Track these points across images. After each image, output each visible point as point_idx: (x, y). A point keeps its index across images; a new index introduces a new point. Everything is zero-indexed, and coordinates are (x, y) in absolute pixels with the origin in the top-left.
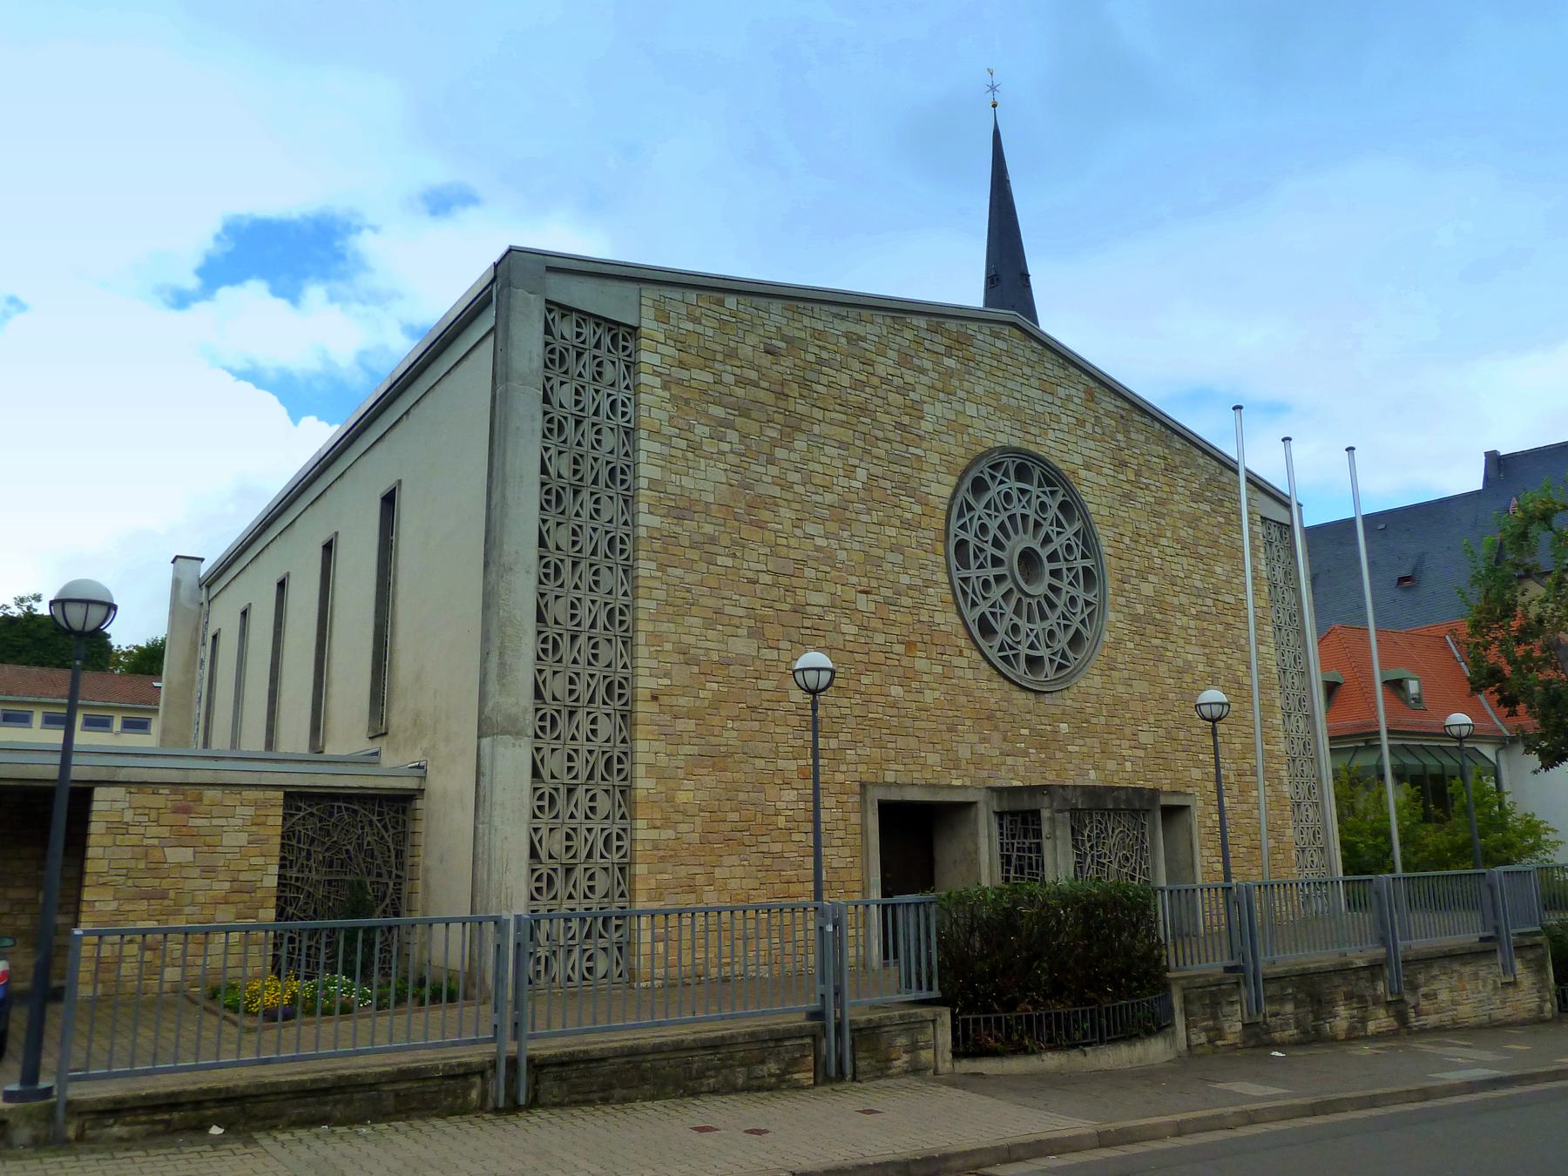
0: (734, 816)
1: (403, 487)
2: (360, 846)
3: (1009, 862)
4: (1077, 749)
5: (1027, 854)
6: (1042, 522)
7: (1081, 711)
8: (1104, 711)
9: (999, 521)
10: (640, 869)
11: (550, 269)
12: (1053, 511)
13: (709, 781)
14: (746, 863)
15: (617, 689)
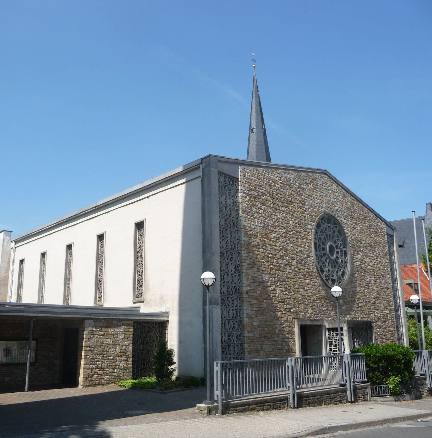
0: (266, 329)
3: (332, 344)
4: (344, 308)
5: (338, 341)
6: (334, 236)
8: (350, 296)
11: (219, 161)
12: (337, 233)
13: (260, 318)
14: (269, 343)
15: (238, 290)
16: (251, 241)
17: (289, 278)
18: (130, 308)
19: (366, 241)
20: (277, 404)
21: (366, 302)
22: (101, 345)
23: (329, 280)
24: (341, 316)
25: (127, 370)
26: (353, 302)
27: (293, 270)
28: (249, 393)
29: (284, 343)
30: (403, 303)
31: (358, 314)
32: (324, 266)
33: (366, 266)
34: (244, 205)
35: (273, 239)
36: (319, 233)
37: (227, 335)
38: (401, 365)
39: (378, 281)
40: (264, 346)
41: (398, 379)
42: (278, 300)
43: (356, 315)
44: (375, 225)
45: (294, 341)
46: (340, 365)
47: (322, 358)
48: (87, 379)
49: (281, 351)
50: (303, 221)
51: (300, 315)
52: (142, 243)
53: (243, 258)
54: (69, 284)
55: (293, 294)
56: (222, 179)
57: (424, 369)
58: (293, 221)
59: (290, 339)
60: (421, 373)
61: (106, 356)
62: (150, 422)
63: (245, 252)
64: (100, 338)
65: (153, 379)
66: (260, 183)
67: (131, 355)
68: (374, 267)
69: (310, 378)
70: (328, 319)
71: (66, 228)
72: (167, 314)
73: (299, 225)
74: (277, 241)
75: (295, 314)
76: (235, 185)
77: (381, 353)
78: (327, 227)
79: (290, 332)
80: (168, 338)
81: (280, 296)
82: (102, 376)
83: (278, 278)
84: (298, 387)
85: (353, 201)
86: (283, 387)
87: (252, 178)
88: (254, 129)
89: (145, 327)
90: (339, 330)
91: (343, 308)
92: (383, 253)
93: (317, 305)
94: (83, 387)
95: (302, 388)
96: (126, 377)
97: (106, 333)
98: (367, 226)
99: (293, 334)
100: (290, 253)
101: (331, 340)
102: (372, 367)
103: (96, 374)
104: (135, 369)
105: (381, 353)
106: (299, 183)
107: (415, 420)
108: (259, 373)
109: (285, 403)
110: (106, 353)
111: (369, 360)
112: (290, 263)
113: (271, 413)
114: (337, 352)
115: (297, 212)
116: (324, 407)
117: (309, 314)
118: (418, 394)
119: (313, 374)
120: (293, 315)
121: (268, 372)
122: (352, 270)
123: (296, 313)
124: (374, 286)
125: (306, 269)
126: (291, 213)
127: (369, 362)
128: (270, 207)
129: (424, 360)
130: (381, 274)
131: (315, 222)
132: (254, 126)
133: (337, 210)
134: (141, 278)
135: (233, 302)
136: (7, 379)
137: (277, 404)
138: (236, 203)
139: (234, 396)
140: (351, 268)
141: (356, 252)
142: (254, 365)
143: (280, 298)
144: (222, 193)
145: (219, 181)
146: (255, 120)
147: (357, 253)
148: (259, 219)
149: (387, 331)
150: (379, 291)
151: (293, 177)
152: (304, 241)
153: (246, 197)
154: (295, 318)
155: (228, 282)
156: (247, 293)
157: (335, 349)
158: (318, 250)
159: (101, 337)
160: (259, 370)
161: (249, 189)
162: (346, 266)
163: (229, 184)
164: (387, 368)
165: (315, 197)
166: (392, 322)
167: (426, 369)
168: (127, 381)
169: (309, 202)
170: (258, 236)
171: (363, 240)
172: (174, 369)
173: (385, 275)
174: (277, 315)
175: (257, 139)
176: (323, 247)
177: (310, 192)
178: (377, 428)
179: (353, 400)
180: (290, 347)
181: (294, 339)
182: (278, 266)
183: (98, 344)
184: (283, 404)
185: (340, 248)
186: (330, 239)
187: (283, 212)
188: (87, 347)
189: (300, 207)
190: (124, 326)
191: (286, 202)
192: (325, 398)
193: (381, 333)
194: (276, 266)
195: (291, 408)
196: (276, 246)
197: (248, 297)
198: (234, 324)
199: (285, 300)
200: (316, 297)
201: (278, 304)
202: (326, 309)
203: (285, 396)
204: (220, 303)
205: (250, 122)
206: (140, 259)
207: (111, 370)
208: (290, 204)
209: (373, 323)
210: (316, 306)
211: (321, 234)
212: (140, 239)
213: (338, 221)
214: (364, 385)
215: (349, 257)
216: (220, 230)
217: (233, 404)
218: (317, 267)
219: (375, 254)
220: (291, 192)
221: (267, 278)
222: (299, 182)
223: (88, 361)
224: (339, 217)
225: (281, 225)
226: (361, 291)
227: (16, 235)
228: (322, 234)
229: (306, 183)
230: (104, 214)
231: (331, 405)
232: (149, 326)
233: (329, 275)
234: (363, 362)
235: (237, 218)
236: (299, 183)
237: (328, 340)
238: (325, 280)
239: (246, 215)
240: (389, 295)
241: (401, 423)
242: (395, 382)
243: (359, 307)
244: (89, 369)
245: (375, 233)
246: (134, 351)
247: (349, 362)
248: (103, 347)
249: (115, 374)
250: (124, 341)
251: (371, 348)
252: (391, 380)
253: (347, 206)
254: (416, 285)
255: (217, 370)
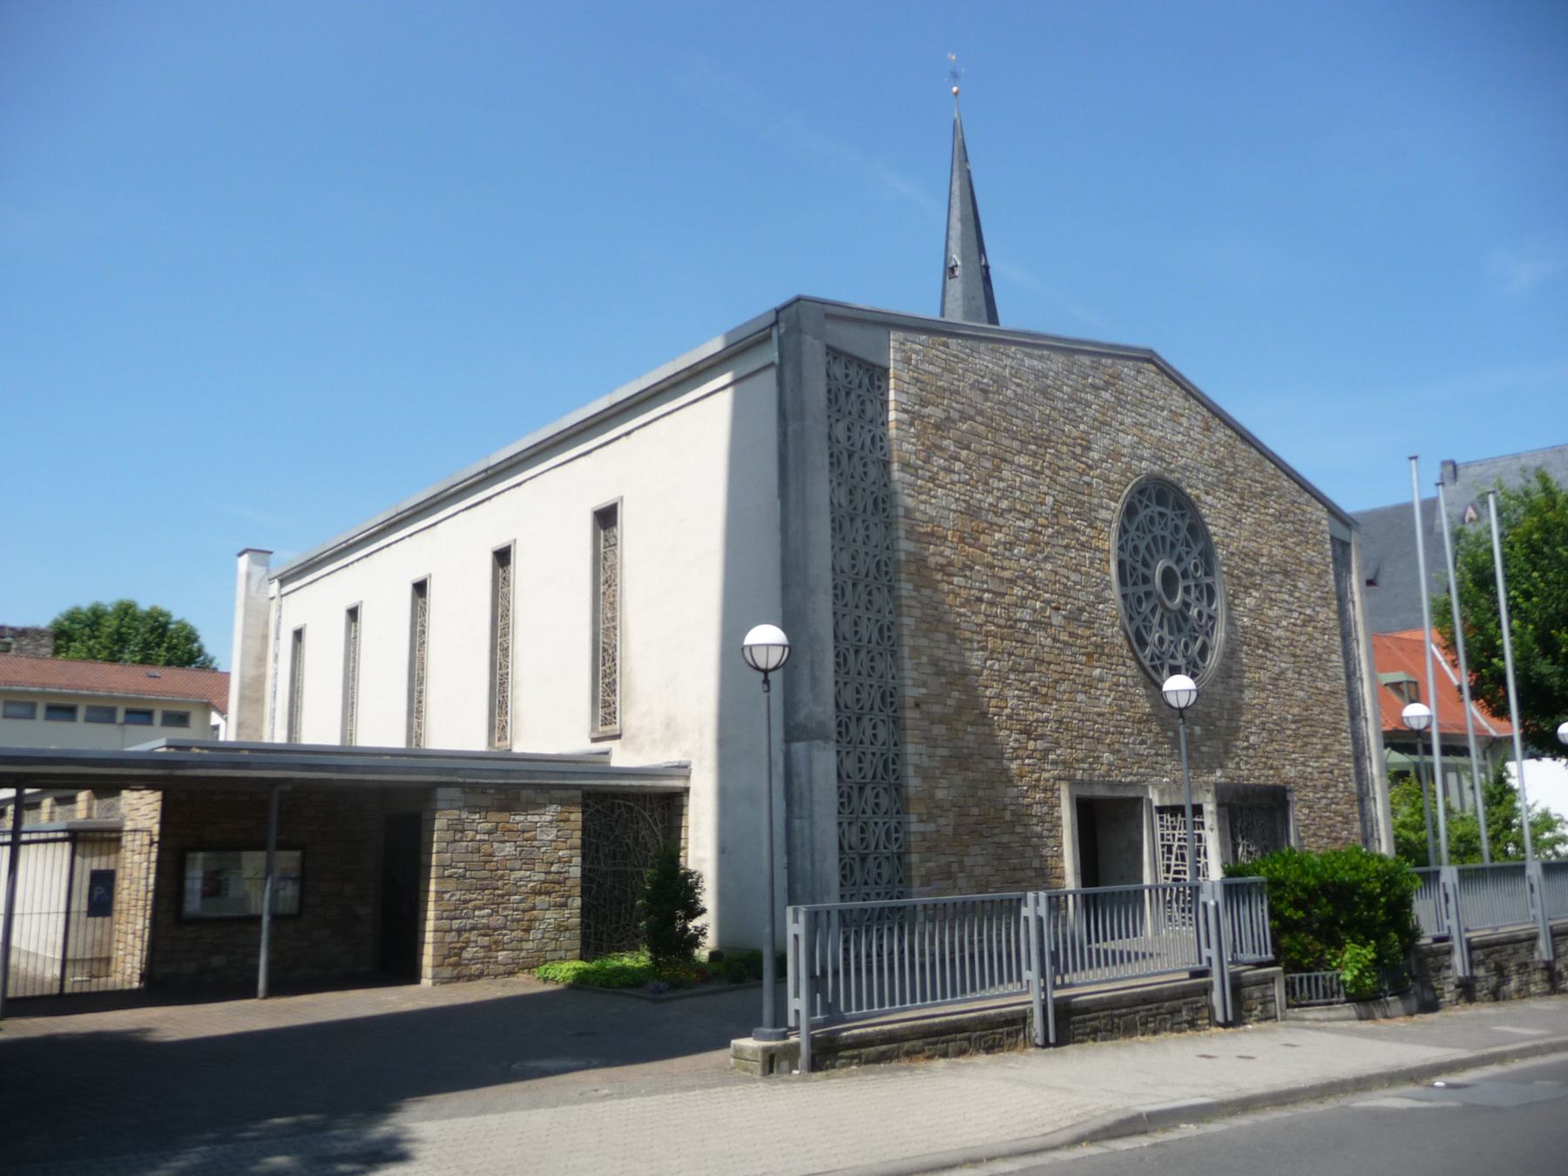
0: (975, 811)
1: (625, 502)
2: (636, 839)
3: (1170, 850)
7: (1208, 714)
9: (1146, 541)
10: (914, 858)
11: (829, 316)
12: (1184, 532)
13: (958, 779)
15: (890, 698)
16: (927, 554)
17: (1043, 661)
18: (582, 756)
19: (1270, 556)
20: (992, 1034)
21: (1270, 731)
22: (486, 862)
23: (1163, 669)
24: (1198, 772)
25: (567, 934)
26: (1233, 731)
27: (1055, 640)
28: (903, 1001)
29: (1029, 852)
30: (1377, 734)
31: (1248, 766)
32: (1149, 629)
33: (1270, 628)
34: (906, 446)
35: (996, 547)
36: (1132, 533)
37: (855, 829)
38: (1376, 912)
39: (1305, 671)
40: (968, 861)
41: (1369, 953)
42: (1012, 725)
43: (1240, 769)
44: (1298, 511)
45: (1060, 845)
46: (1190, 912)
47: (1143, 892)
48: (447, 961)
49: (1019, 875)
50: (1086, 498)
51: (1076, 769)
52: (613, 567)
53: (904, 602)
54: (421, 692)
55: (1056, 710)
56: (838, 370)
57: (1447, 923)
58: (1054, 496)
59: (1048, 837)
60: (1436, 933)
61: (500, 892)
62: (567, 1101)
63: (910, 586)
64: (484, 841)
65: (637, 960)
66: (955, 382)
67: (579, 889)
68: (1293, 632)
69: (1106, 952)
70: (1161, 782)
71: (410, 535)
72: (683, 769)
73: (1072, 510)
74: (1007, 553)
75: (1061, 767)
76: (879, 387)
77: (1316, 876)
78: (1156, 517)
79: (1048, 818)
80: (687, 838)
81: (1017, 714)
82: (490, 950)
83: (1010, 663)
84: (1059, 981)
85: (1231, 441)
86: (1010, 980)
87: (931, 368)
88: (956, 266)
89: (620, 808)
90: (1188, 812)
91: (1204, 749)
92: (1318, 593)
93: (1126, 741)
94: (434, 984)
95: (1071, 985)
96: (562, 953)
97: (500, 825)
98: (1272, 515)
99: (1056, 825)
100: (1046, 588)
101: (1169, 840)
102: (1290, 918)
103: (472, 945)
104: (592, 931)
105: (1316, 876)
106: (1071, 387)
107: (1425, 1082)
108: (954, 936)
109: (1017, 1032)
110: (500, 883)
111: (1281, 899)
112: (1046, 620)
113: (972, 1064)
114: (1185, 874)
115: (1068, 469)
116: (1143, 1042)
117: (1105, 768)
118: (1428, 996)
119: (1113, 938)
120: (1055, 767)
121: (980, 934)
122: (1228, 640)
123: (1064, 762)
124: (1294, 685)
125: (1094, 635)
126: (1047, 472)
127: (1281, 902)
128: (986, 453)
129: (1446, 896)
130: (1315, 652)
131: (1121, 500)
132: (956, 259)
133: (1185, 468)
134: (613, 669)
135: (874, 732)
136: (217, 961)
137: (992, 1034)
138: (881, 440)
139: (854, 1012)
140: (1228, 635)
141: (1242, 589)
142: (936, 913)
143: (1017, 720)
144: (839, 411)
145: (828, 375)
146: (959, 243)
147: (1245, 592)
148: (951, 490)
149: (1332, 815)
150: (1310, 701)
151: (1055, 368)
152: (1087, 555)
153: (912, 424)
154: (1059, 779)
155: (859, 674)
156: (917, 705)
157: (1181, 868)
158: (1130, 582)
159: (486, 837)
160: (952, 929)
161: (921, 400)
162: (1212, 628)
163: (860, 386)
164: (1333, 921)
165: (1121, 428)
166: (1346, 788)
167: (1452, 922)
168: (562, 966)
169: (1101, 442)
170: (950, 538)
171: (1262, 555)
172: (703, 929)
173: (1325, 656)
174: (1008, 769)
175: (965, 296)
176: (1143, 574)
177: (1103, 414)
178: (1305, 1111)
179: (1230, 1018)
180: (1046, 861)
181: (1058, 839)
182: (1011, 627)
183: (476, 857)
184: (1009, 1035)
185: (1194, 577)
186: (1164, 548)
187: (1023, 470)
188: (445, 867)
189: (1075, 456)
190: (555, 806)
191: (1032, 441)
192: (1143, 1013)
193: (1314, 820)
194: (1005, 627)
195: (1037, 1046)
196: (1003, 568)
197: (918, 716)
198: (877, 796)
199: (1030, 725)
200: (1123, 718)
201: (1010, 737)
202: (1153, 752)
203: (1018, 1012)
204: (835, 736)
205: (947, 249)
206: (609, 615)
207: (519, 934)
208: (1046, 448)
209: (1290, 791)
210: (1124, 743)
211: (1139, 537)
212: (610, 555)
213: (1188, 497)
214: (1265, 974)
215: (1219, 604)
216: (833, 521)
217: (847, 1037)
218: (1125, 631)
219: (1297, 594)
220: (1048, 412)
221: (976, 662)
222: (1071, 383)
223: (445, 908)
224: (1191, 487)
225: (1018, 507)
226: (1256, 701)
227: (287, 558)
228: (1142, 535)
229: (1093, 386)
230: (509, 488)
231: (1162, 1036)
232: (631, 804)
233: (1163, 653)
234: (1262, 902)
235: (885, 485)
236: (1071, 387)
237: (1160, 842)
238: (1150, 669)
239: (912, 475)
240: (1337, 712)
241: (1381, 1092)
242: (1358, 962)
243: (1251, 747)
244: (451, 930)
245: (1296, 534)
246: (586, 877)
247: (1217, 904)
248: (492, 866)
249: (530, 945)
250: (557, 849)
251: (1286, 862)
252: (1347, 956)
253: (1215, 457)
254: (1412, 686)
255: (797, 933)
